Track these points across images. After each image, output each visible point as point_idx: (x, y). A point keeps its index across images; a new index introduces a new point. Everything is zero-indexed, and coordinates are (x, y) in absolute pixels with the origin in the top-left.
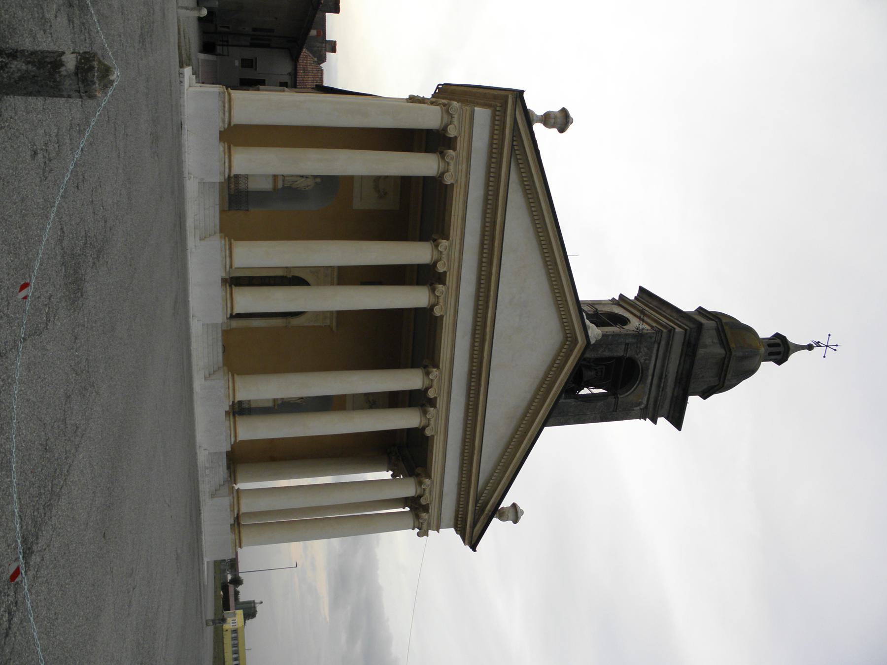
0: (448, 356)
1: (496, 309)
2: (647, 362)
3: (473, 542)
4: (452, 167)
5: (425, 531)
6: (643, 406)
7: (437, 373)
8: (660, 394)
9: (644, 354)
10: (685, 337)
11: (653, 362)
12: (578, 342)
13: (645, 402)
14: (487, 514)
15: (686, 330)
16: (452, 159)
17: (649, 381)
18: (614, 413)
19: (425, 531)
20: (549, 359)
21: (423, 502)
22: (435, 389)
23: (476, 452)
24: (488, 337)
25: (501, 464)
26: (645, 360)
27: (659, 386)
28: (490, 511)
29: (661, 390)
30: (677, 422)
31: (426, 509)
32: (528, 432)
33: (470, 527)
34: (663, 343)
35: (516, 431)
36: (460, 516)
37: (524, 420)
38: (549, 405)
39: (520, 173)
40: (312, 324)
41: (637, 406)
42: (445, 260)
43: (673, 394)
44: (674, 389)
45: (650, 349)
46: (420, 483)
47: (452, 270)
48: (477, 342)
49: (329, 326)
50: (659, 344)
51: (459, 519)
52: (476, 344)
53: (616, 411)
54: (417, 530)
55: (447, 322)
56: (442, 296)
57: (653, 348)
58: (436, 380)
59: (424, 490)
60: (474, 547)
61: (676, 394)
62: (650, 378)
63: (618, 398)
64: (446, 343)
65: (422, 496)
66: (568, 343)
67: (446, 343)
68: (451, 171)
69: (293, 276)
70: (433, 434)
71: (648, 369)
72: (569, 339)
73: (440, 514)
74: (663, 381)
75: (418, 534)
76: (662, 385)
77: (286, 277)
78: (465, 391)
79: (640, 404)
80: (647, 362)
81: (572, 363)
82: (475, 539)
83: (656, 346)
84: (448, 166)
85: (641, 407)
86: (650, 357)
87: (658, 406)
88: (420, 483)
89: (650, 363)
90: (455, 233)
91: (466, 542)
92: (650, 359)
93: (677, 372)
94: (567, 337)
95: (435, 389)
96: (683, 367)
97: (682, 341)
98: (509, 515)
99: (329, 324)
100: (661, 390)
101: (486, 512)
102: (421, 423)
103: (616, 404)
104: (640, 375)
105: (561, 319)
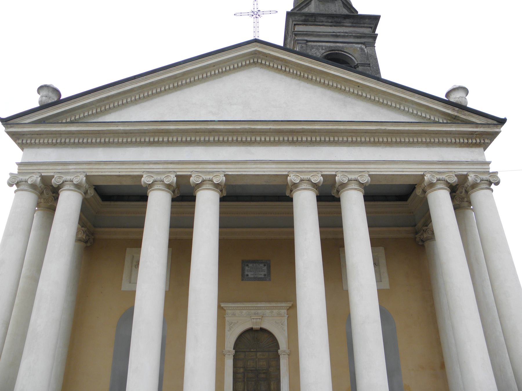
0: (274, 166)
1: (214, 121)
2: (324, 48)
3: (495, 122)
4: (68, 178)
5: (490, 176)
6: (363, 47)
7: (292, 175)
8: (350, 34)
9: (317, 51)
10: (301, 25)
11: (324, 44)
12: (256, 50)
13: (360, 46)
14: (458, 112)
15: (295, 25)
16: (60, 177)
17: (341, 45)
18: (371, 66)
19: (490, 176)
20: (279, 77)
21: (454, 180)
22: (312, 176)
23: (383, 128)
24: (247, 126)
25: (398, 106)
26: (322, 49)
27: (344, 37)
28: (454, 110)
29: (346, 34)
30: (375, 19)
31: (463, 178)
32: (358, 83)
33: (477, 127)
34: (306, 38)
35: (359, 97)
36: (466, 141)
37: (345, 90)
38: (323, 66)
39: (116, 108)
40: (286, 328)
41: (364, 51)
42: (163, 177)
43: (350, 27)
44: (346, 26)
45: (312, 47)
46: (431, 185)
47: (175, 170)
48: (255, 139)
49: (288, 310)
50: (307, 41)
51: (470, 141)
52: (258, 139)
53: (370, 64)
54: (493, 186)
55: (233, 170)
56: (203, 176)
57: (311, 45)
58: (301, 176)
59: (438, 180)
60: (502, 122)
61: (350, 25)
62: (338, 44)
63: (357, 64)
64: (258, 170)
65: (447, 181)
66: (260, 61)
67: (258, 170)
68: (72, 177)
69: (234, 349)
70: (367, 175)
71: (330, 47)
72: (256, 60)
73: (467, 163)
74: (338, 34)
75: (497, 184)
76: (343, 34)
77: (234, 356)
78: (315, 147)
79: (362, 49)
80: (324, 48)
81: (279, 53)
82: (490, 121)
83: (310, 43)
84: (67, 181)
85: (365, 47)
86: (319, 46)
87: (361, 35)
88: (431, 185)
89: (325, 46)
90: (137, 170)
91: (497, 130)
92: (322, 46)
93: (331, 26)
94: (254, 62)
95: (312, 176)
96: (326, 22)
97: (304, 26)
98: (458, 96)
99: (286, 311)
100: (346, 34)
101: (456, 114)
102: (356, 189)
103: (363, 65)
104: (336, 52)
105: (235, 70)
